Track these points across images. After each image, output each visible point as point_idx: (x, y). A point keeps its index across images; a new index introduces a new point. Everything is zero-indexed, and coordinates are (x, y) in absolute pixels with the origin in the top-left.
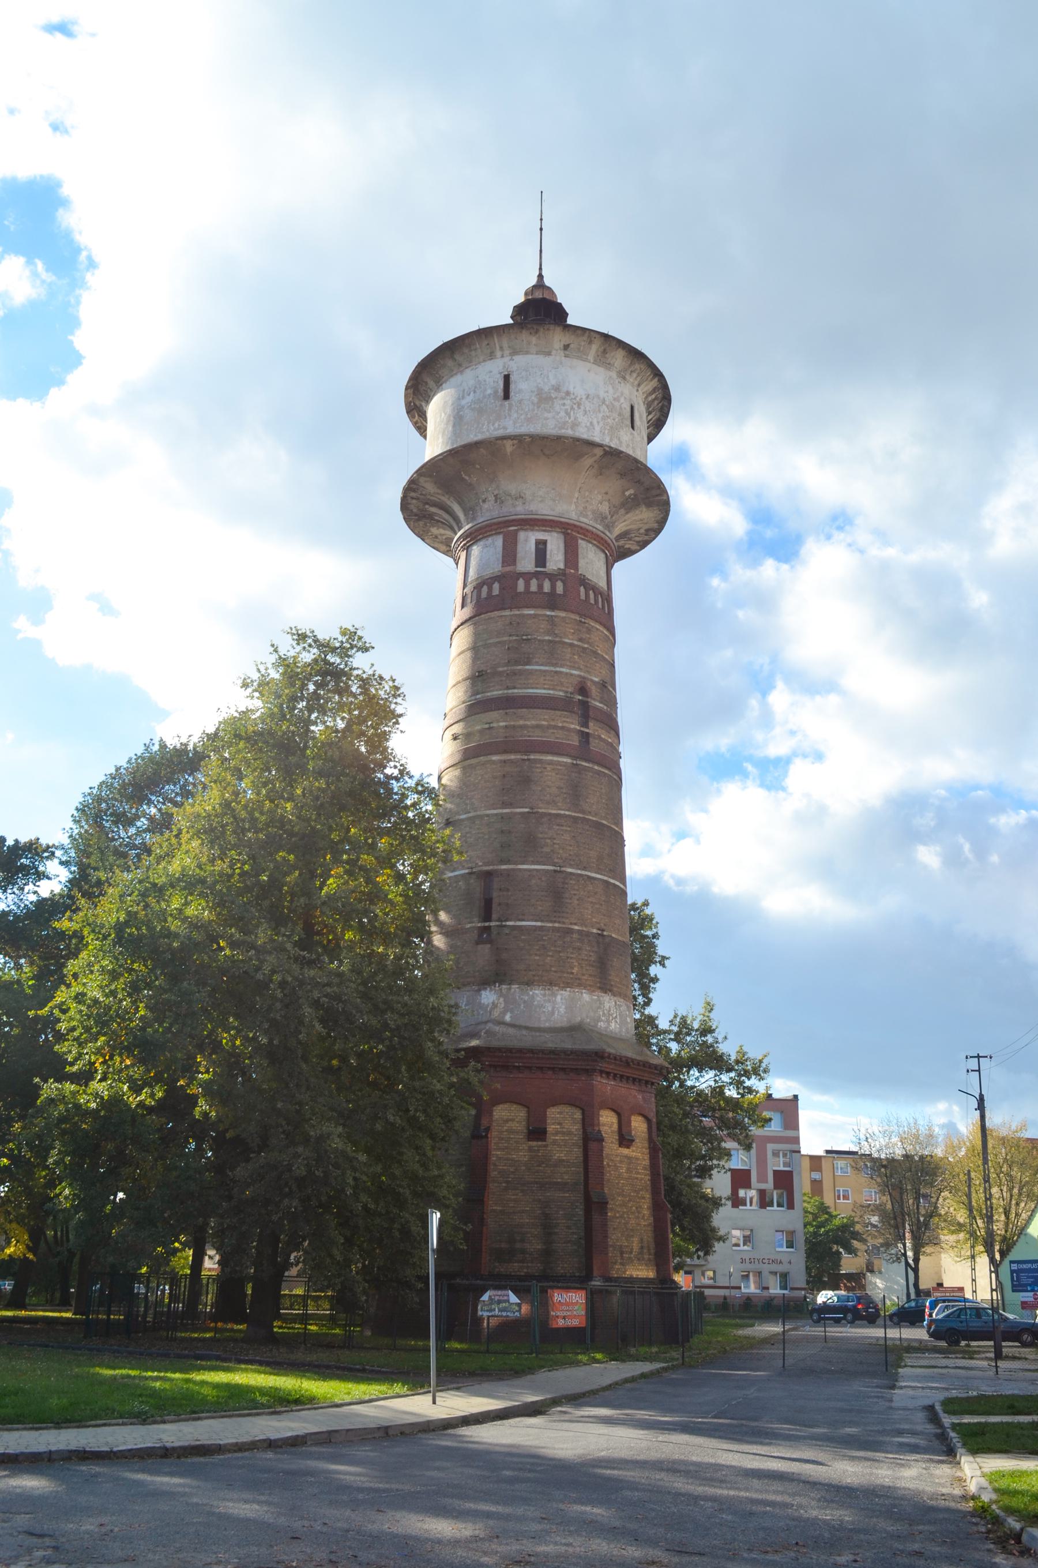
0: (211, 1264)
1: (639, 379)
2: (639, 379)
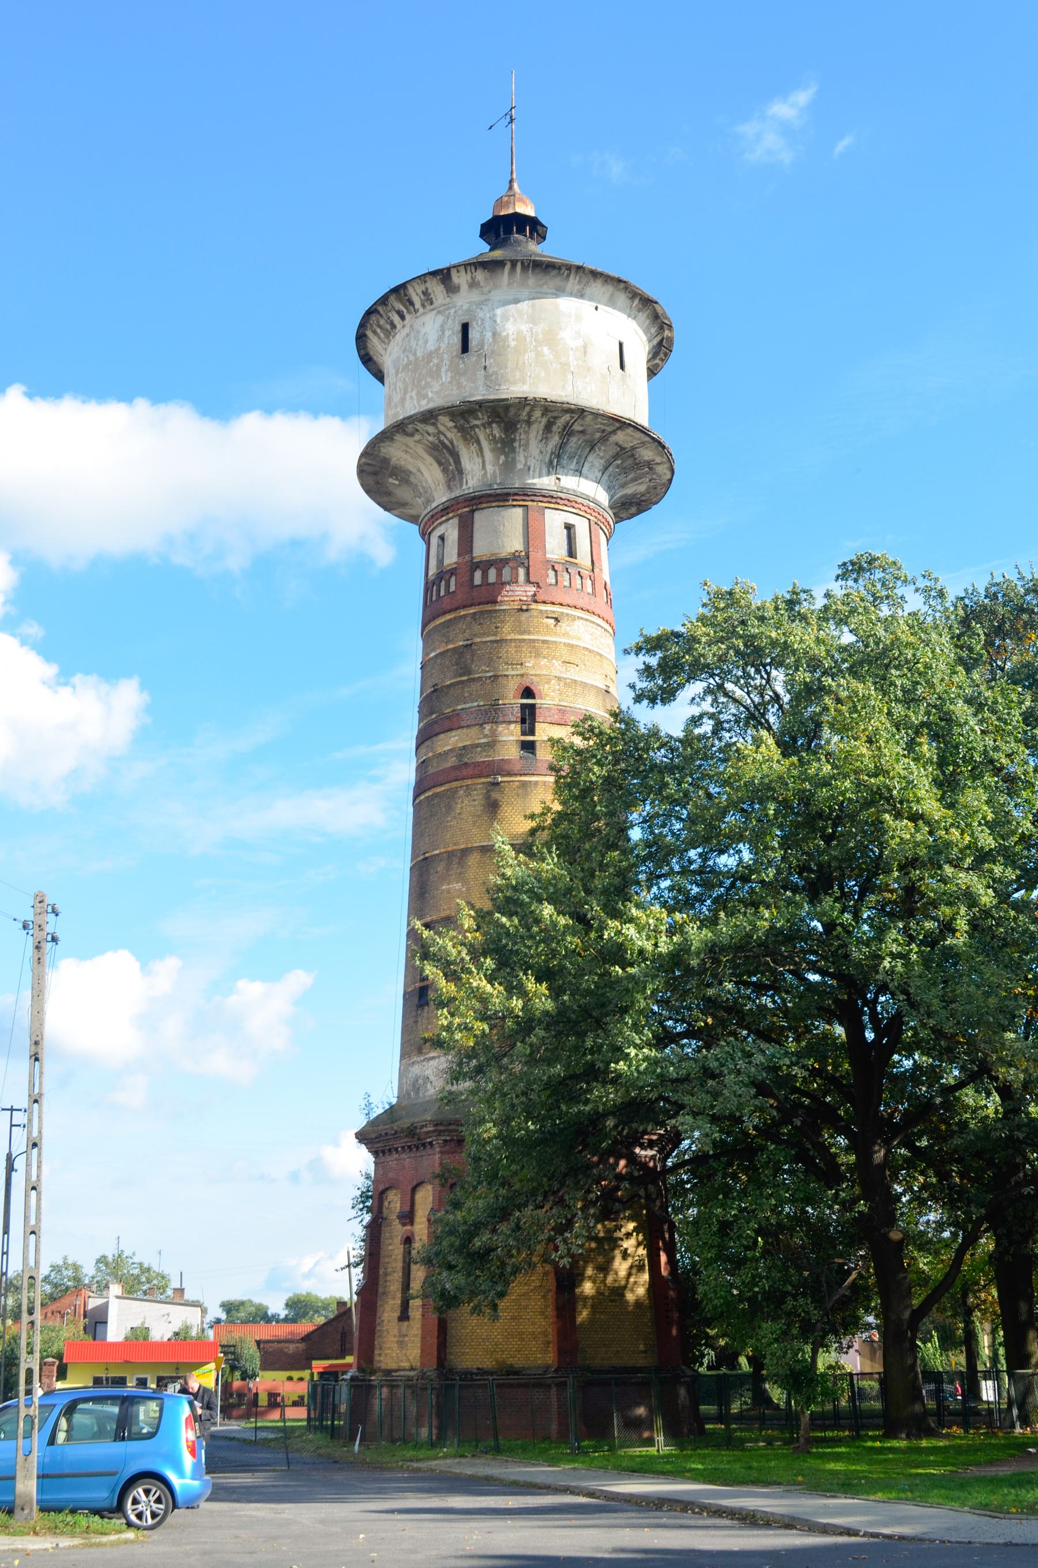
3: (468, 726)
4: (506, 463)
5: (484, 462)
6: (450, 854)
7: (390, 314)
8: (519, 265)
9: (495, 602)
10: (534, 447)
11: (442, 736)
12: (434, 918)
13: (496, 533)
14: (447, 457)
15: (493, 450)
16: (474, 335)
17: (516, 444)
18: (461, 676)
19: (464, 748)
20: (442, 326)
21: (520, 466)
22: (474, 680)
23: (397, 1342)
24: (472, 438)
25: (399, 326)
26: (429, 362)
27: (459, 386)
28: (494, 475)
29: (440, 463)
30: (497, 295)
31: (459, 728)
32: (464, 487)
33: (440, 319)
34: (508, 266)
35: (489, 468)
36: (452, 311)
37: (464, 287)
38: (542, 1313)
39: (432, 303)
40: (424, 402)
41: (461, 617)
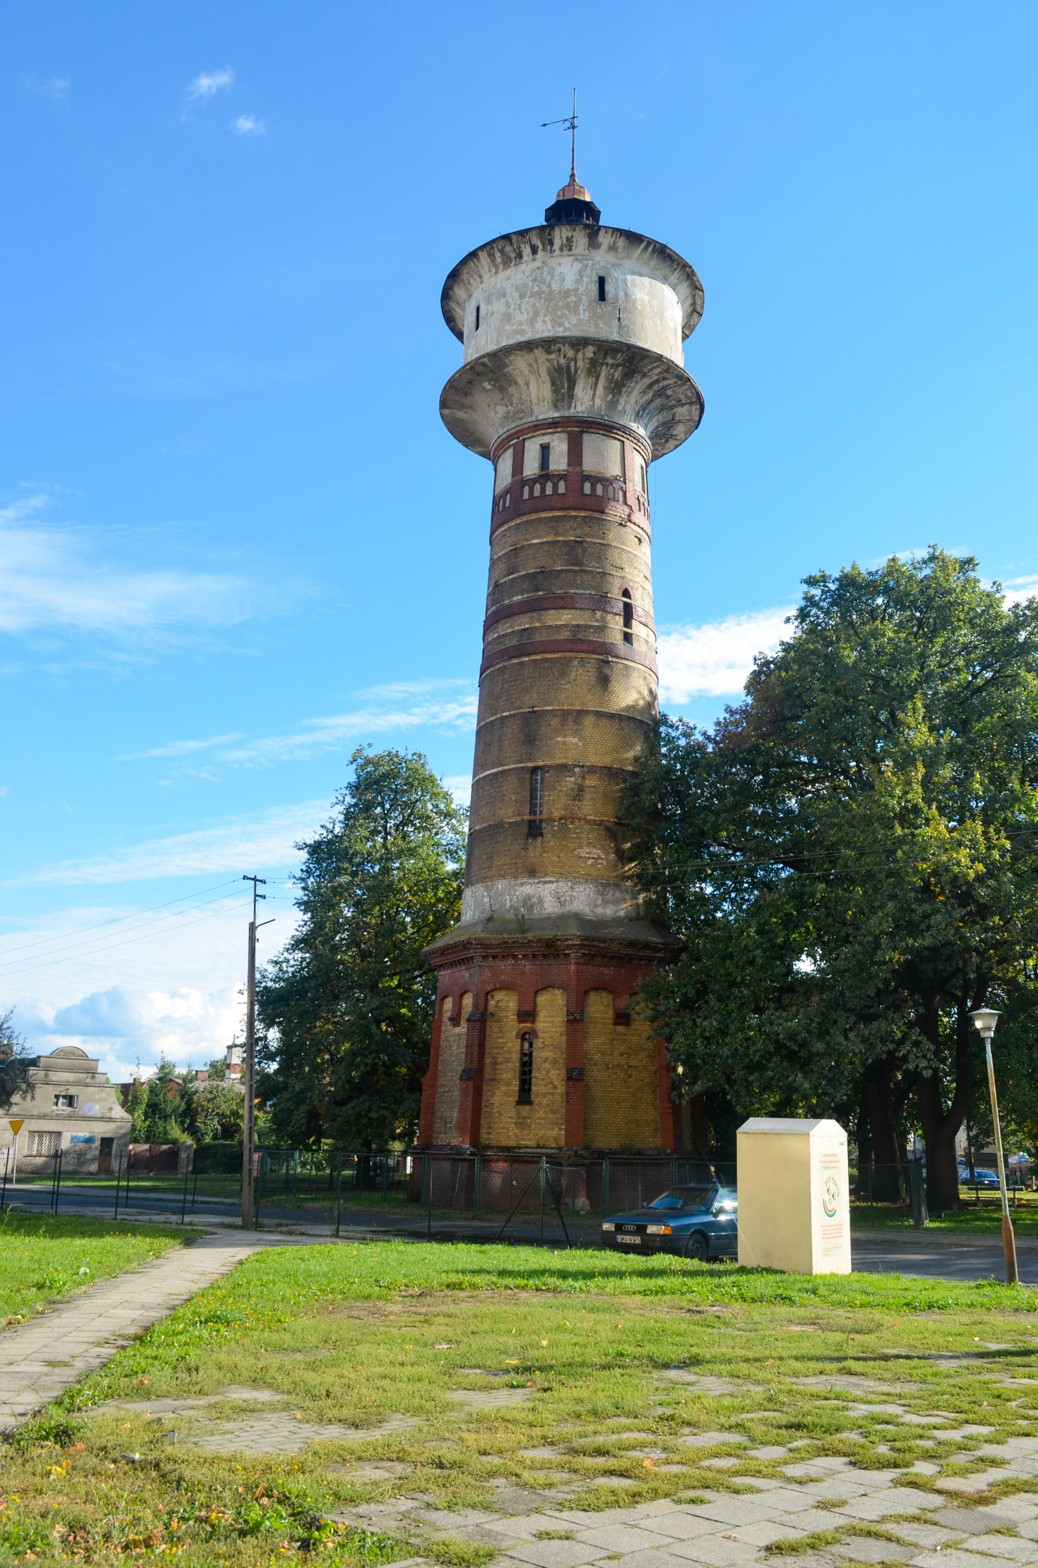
0: (1010, 875)
1: (475, 276)
2: (475, 276)
3: (582, 609)
4: (611, 401)
5: (594, 395)
6: (565, 714)
7: (522, 246)
8: (652, 246)
9: (603, 512)
10: (634, 396)
11: (552, 611)
12: (548, 763)
13: (601, 455)
14: (563, 381)
15: (605, 388)
16: (609, 288)
17: (624, 389)
18: (572, 565)
19: (578, 626)
20: (580, 272)
21: (620, 408)
22: (585, 571)
23: (516, 1123)
24: (595, 372)
25: (525, 258)
26: (566, 297)
27: (597, 326)
28: (600, 407)
29: (553, 384)
30: (627, 264)
31: (573, 608)
32: (572, 410)
33: (578, 266)
34: (644, 244)
35: (598, 401)
36: (590, 263)
37: (604, 247)
38: (653, 1104)
39: (570, 250)
40: (561, 329)
41: (572, 516)
